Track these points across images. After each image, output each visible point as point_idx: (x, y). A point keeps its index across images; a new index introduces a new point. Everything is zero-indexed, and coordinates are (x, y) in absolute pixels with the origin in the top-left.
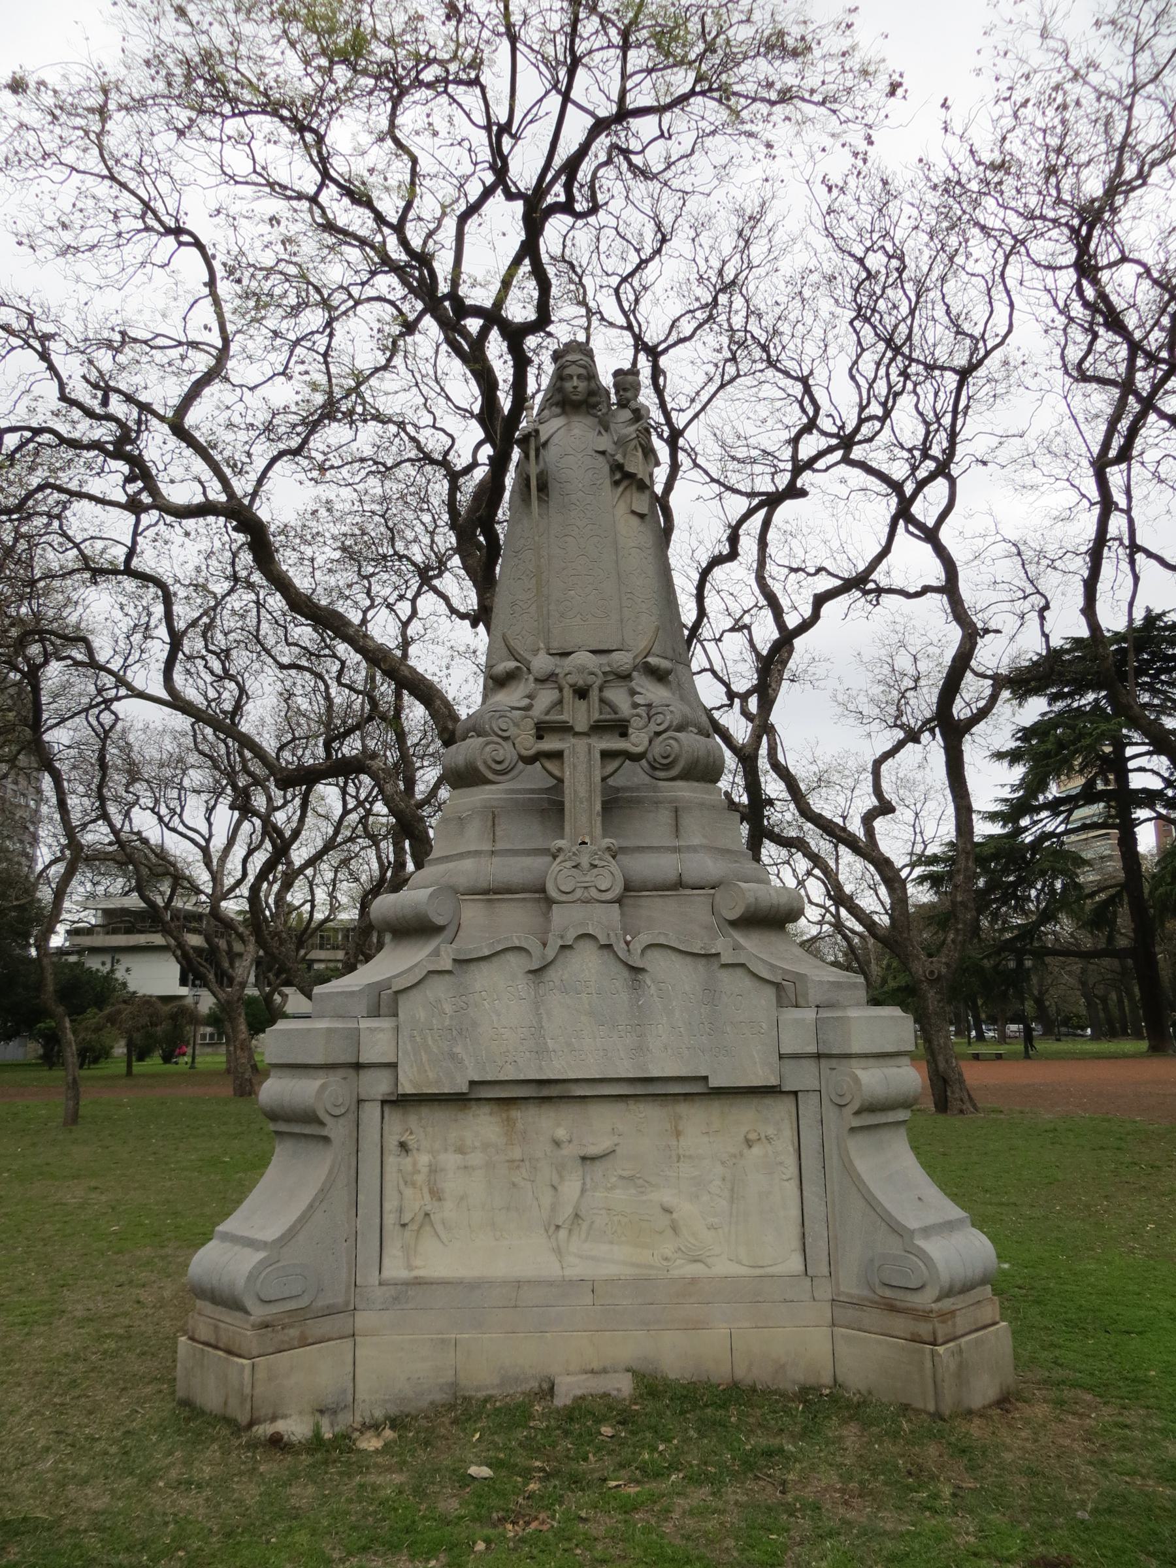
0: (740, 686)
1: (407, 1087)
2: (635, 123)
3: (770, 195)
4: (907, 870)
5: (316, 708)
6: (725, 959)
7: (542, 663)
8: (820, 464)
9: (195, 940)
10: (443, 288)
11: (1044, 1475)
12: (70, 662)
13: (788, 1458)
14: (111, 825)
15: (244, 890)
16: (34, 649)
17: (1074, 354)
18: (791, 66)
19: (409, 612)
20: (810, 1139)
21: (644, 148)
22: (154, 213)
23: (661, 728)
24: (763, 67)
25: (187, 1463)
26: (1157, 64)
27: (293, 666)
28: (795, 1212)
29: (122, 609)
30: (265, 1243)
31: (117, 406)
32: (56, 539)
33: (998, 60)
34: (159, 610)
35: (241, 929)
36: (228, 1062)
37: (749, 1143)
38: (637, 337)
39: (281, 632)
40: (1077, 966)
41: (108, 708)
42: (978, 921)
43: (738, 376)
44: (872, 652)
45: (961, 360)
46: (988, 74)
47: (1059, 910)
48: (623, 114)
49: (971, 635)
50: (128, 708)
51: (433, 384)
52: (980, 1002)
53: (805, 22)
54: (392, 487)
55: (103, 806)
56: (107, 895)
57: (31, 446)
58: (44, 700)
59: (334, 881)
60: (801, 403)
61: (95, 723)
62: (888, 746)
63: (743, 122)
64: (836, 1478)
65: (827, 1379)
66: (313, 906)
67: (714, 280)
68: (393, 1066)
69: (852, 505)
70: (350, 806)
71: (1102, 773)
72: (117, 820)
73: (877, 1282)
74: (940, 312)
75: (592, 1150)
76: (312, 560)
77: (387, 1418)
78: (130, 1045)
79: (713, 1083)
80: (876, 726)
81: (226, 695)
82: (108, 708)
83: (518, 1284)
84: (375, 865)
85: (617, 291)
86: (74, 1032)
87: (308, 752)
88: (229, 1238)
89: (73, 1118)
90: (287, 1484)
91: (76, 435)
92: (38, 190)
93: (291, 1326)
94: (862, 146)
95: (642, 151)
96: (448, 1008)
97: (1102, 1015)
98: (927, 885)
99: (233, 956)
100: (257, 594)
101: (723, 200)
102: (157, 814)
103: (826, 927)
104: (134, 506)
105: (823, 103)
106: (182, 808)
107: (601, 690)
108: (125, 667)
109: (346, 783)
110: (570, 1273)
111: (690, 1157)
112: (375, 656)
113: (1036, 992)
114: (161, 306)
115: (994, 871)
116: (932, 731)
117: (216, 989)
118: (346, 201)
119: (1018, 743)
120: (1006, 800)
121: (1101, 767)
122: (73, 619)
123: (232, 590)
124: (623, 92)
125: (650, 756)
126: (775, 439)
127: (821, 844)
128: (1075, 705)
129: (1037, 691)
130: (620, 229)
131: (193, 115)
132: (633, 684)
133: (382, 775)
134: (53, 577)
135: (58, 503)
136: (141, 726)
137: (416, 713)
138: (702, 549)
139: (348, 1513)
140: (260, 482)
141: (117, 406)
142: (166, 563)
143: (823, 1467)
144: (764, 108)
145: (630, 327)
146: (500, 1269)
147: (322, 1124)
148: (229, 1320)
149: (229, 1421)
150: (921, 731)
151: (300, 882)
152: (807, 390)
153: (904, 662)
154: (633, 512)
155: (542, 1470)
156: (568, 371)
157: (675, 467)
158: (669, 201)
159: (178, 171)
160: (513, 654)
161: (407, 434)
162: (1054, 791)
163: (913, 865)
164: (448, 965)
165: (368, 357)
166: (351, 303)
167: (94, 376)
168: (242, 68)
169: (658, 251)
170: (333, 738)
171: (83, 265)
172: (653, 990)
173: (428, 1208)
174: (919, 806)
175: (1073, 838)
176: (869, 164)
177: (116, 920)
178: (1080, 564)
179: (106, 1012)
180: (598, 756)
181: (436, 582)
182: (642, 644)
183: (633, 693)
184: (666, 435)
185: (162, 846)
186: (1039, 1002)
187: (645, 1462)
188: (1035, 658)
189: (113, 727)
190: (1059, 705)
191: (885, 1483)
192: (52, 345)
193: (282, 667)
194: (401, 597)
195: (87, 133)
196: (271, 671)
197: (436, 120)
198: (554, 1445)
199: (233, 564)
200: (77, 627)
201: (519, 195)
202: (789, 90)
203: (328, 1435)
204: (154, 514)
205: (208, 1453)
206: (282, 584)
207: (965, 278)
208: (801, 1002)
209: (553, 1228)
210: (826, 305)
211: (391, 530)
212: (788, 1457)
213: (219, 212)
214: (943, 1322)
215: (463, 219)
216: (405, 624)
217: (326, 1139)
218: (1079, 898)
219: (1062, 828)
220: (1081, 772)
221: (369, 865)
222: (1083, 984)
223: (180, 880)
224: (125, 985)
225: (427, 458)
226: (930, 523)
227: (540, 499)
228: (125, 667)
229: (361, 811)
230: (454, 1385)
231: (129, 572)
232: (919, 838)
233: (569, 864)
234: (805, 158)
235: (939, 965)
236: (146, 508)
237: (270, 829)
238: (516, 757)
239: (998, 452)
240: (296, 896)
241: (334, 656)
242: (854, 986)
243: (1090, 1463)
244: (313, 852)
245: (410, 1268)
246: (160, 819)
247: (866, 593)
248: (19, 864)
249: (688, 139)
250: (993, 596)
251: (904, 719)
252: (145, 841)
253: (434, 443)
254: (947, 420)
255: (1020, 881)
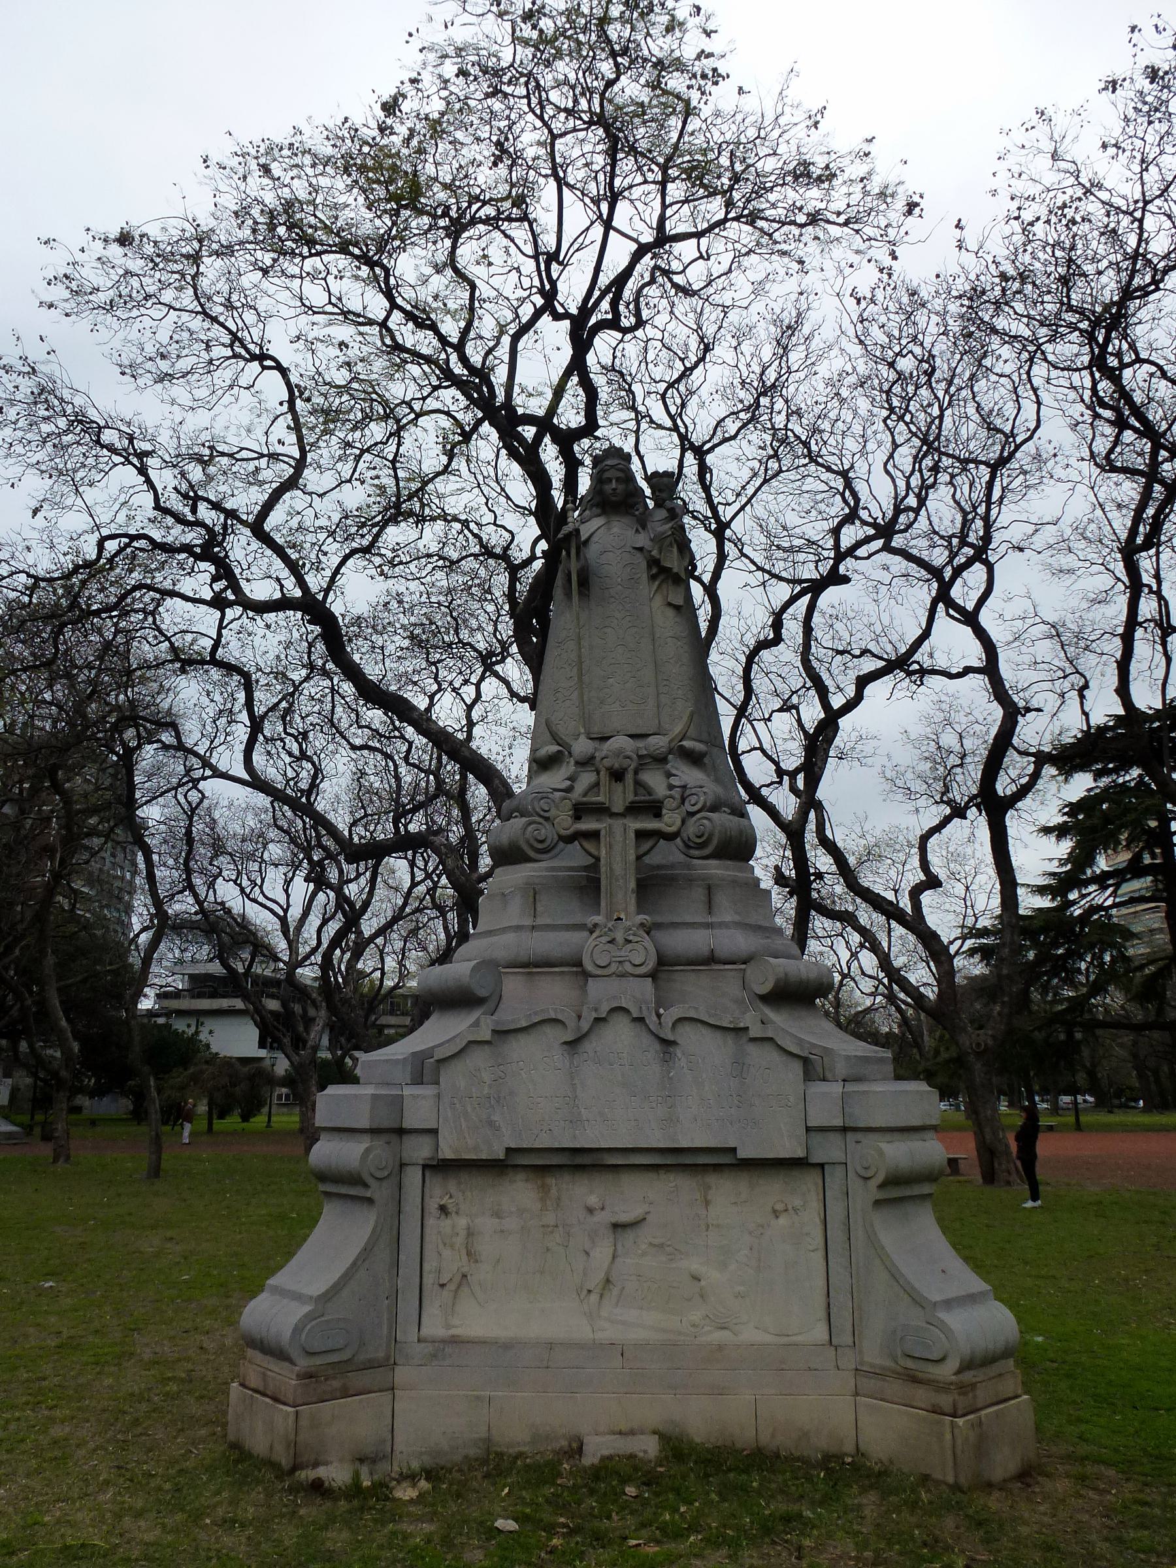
0: (790, 764)
1: (447, 1153)
2: (678, 247)
3: (805, 307)
4: (959, 942)
5: (386, 786)
6: (753, 1033)
7: (582, 746)
8: (862, 552)
9: (273, 1005)
10: (500, 397)
11: (1059, 1551)
12: (159, 745)
13: (805, 1524)
14: (196, 895)
15: (318, 958)
16: (130, 733)
17: (1102, 446)
18: (815, 192)
19: (473, 696)
20: (836, 1211)
21: (685, 268)
22: (241, 341)
23: (695, 808)
24: (788, 195)
25: (234, 1502)
26: (1163, 180)
27: (365, 747)
28: (821, 1282)
29: (208, 695)
30: (311, 1297)
31: (205, 513)
32: (151, 634)
33: (1013, 182)
34: (241, 696)
35: (314, 995)
36: (302, 1121)
37: (776, 1214)
38: (683, 438)
39: (353, 716)
40: (1127, 1038)
41: (195, 787)
42: (1026, 993)
43: (781, 471)
44: (918, 730)
45: (993, 455)
46: (1004, 195)
47: (1109, 984)
48: (663, 239)
49: (1012, 713)
50: (211, 787)
51: (494, 485)
52: (1032, 1074)
53: (828, 153)
54: (458, 579)
55: (188, 879)
56: (193, 961)
57: (129, 550)
58: (137, 779)
59: (403, 949)
60: (843, 495)
61: (182, 801)
62: (936, 821)
63: (776, 242)
64: (851, 1545)
65: (849, 1447)
66: (383, 974)
67: (755, 384)
68: (434, 1132)
69: (895, 590)
70: (418, 879)
71: (1149, 847)
72: (202, 891)
73: (899, 1353)
74: (971, 410)
75: (624, 1218)
76: (382, 648)
77: (423, 1469)
78: (210, 1105)
79: (742, 1154)
80: (922, 802)
81: (304, 774)
82: (195, 787)
83: (551, 1346)
84: (443, 936)
85: (663, 397)
86: (159, 1091)
87: (379, 827)
88: (277, 1290)
89: (155, 1172)
90: (325, 1528)
91: (170, 539)
92: (141, 326)
93: (334, 1378)
94: (887, 261)
95: (683, 271)
96: (487, 1077)
97: (1153, 1087)
98: (977, 957)
99: (309, 1022)
100: (331, 680)
101: (763, 310)
102: (240, 885)
103: (879, 999)
104: (218, 603)
105: (846, 223)
106: (263, 880)
107: (636, 772)
108: (211, 749)
109: (414, 857)
110: (599, 1336)
111: (718, 1226)
112: (440, 739)
113: (1088, 1064)
114: (246, 422)
115: (1043, 944)
116: (978, 806)
117: (289, 1051)
118: (411, 325)
119: (1065, 818)
120: (1053, 874)
121: (1147, 841)
122: (165, 705)
123: (307, 678)
124: (662, 219)
125: (684, 835)
126: (817, 530)
127: (867, 916)
128: (1121, 780)
129: (1083, 768)
130: (666, 341)
131: (275, 256)
132: (668, 766)
133: (443, 850)
134: (149, 668)
135: (153, 600)
136: (226, 803)
137: (479, 793)
138: (749, 635)
139: (378, 1558)
140: (332, 580)
141: (205, 513)
142: (249, 652)
143: (839, 1534)
144: (796, 231)
145: (675, 428)
146: (537, 1330)
147: (366, 1186)
148: (276, 1370)
149: (273, 1465)
150: (967, 807)
151: (371, 950)
152: (848, 484)
153: (949, 739)
154: (670, 604)
155: (565, 1525)
156: (607, 475)
157: (722, 557)
158: (712, 315)
159: (263, 304)
160: (556, 738)
161: (471, 531)
162: (1102, 864)
163: (964, 938)
164: (487, 1036)
165: (433, 460)
166: (412, 416)
167: (184, 487)
168: (319, 214)
169: (702, 359)
170: (400, 814)
171: (178, 391)
172: (683, 1062)
173: (465, 1270)
174: (969, 879)
175: (1124, 911)
176: (894, 278)
177: (201, 985)
178: (1115, 647)
179: (191, 1071)
180: (633, 835)
181: (498, 668)
182: (678, 729)
183: (669, 775)
184: (713, 526)
185: (243, 916)
186: (1092, 1074)
187: (666, 1522)
188: (1079, 736)
189: (198, 804)
190: (1105, 781)
191: (901, 1554)
192: (151, 462)
193: (354, 748)
194: (466, 682)
195: (183, 276)
196: (345, 751)
197: (490, 251)
198: (579, 1503)
199: (309, 653)
200: (169, 712)
201: (567, 315)
202: (818, 212)
203: (366, 1483)
204: (238, 610)
205: (254, 1494)
206: (353, 673)
207: (993, 378)
208: (829, 1075)
209: (585, 1292)
210: (863, 405)
211: (455, 619)
212: (807, 1524)
213: (299, 338)
214: (965, 1394)
215: (516, 338)
216: (470, 708)
217: (370, 1201)
218: (1127, 971)
219: (1109, 902)
220: (1128, 847)
221: (436, 935)
222: (1135, 1056)
223: (261, 948)
224: (208, 1046)
225: (487, 551)
226: (970, 606)
227: (580, 593)
228: (211, 749)
229: (429, 883)
230: (488, 1440)
231: (215, 662)
232: (970, 911)
233: (604, 939)
234: (835, 272)
235: (985, 1037)
236: (231, 604)
237: (342, 900)
238: (556, 837)
239: (1035, 538)
240: (367, 964)
241: (402, 737)
242: (881, 1060)
243: (1106, 1539)
244: (383, 921)
245: (448, 1326)
246: (242, 890)
247: (909, 674)
248: (116, 931)
249: (727, 259)
250: (1034, 676)
251: (951, 795)
252: (228, 911)
253: (496, 539)
254: (981, 510)
255: (1069, 954)
